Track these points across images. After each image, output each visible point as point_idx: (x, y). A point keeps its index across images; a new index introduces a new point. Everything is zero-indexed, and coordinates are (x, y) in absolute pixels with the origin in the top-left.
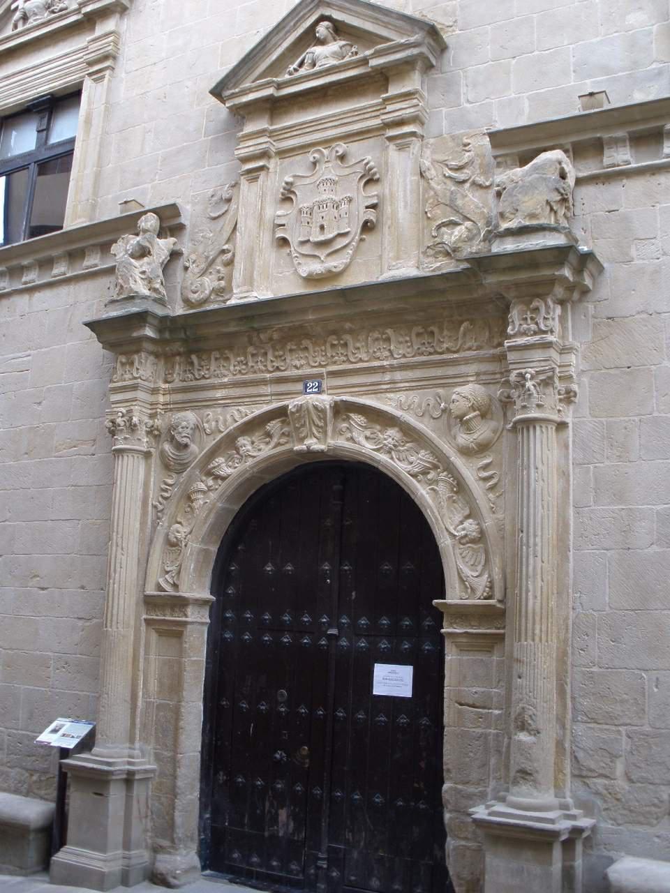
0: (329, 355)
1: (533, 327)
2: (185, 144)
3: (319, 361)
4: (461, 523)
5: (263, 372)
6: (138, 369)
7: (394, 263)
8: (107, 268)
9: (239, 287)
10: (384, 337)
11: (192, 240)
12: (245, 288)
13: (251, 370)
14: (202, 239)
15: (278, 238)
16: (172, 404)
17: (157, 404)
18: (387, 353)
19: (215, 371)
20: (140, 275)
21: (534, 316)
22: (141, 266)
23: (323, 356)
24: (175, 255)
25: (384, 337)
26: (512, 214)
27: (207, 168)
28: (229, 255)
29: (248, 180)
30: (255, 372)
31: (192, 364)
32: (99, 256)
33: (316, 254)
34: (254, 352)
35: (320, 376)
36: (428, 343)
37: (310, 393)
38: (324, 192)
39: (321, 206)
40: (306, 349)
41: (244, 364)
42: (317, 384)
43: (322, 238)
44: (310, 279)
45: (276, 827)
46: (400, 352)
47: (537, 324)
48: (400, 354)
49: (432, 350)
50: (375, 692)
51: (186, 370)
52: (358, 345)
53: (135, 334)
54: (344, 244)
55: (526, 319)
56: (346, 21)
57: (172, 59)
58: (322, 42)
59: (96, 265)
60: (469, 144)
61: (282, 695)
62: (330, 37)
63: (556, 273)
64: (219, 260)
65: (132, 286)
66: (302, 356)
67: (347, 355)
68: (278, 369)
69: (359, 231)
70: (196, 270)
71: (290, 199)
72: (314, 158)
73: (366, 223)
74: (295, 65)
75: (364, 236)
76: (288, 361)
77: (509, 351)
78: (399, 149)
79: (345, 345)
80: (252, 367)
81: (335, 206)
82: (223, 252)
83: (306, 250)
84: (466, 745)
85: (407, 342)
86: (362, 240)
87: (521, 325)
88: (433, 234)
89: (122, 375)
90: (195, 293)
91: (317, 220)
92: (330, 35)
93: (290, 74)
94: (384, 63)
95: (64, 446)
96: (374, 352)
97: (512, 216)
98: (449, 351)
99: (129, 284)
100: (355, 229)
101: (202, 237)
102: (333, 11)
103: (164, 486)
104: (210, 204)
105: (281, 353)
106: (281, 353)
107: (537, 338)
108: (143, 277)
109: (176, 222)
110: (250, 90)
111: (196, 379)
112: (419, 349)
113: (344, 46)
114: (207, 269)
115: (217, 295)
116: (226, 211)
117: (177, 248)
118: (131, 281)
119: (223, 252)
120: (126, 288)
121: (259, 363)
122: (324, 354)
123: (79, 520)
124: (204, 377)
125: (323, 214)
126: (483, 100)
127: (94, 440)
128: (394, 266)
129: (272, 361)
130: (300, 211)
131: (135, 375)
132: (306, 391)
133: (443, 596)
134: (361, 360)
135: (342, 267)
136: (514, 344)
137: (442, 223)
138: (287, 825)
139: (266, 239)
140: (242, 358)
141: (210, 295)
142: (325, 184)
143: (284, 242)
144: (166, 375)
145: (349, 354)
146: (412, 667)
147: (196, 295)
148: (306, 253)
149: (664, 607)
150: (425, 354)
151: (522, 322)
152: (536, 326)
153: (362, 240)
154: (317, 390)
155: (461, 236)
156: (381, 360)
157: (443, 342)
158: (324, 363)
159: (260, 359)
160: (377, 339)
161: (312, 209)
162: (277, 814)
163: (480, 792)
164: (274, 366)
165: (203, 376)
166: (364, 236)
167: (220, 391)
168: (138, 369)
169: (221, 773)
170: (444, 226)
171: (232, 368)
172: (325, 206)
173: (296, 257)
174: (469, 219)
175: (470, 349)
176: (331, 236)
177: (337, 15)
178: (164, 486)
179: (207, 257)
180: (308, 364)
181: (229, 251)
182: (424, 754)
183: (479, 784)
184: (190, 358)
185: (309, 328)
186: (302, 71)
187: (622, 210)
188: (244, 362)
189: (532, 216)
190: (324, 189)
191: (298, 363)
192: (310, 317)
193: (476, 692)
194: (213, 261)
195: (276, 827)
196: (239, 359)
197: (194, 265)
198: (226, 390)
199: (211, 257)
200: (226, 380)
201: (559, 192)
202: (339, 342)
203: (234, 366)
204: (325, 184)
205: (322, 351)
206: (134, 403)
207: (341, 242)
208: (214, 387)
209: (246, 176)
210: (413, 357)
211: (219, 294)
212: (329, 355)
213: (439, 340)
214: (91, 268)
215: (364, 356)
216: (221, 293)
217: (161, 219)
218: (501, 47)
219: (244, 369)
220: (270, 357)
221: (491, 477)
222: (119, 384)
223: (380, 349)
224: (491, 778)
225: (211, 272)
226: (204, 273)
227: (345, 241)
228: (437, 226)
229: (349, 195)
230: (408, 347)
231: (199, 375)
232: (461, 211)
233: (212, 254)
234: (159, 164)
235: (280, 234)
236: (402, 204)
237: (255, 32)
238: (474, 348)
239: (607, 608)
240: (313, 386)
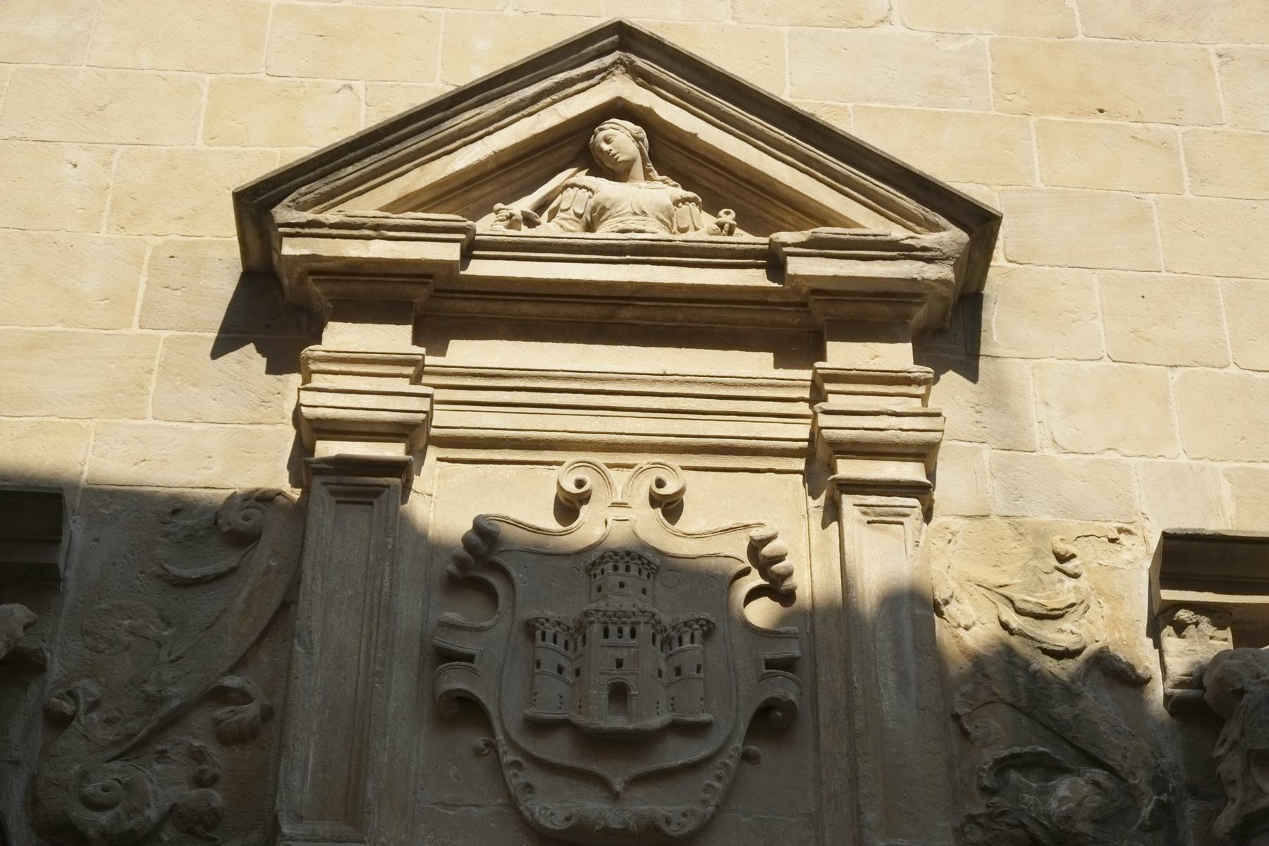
9: (299, 818)
11: (84, 633)
27: (150, 421)
28: (251, 711)
29: (333, 493)
33: (596, 768)
38: (618, 590)
43: (617, 722)
54: (696, 757)
58: (616, 172)
60: (1073, 556)
69: (743, 728)
70: (105, 735)
72: (580, 483)
73: (765, 711)
78: (869, 522)
81: (659, 638)
82: (220, 695)
83: (557, 749)
86: (748, 757)
88: (986, 782)
90: (101, 807)
94: (835, 278)
101: (132, 632)
104: (167, 535)
109: (476, 539)
114: (145, 742)
116: (232, 571)
125: (621, 654)
126: (1100, 453)
130: (530, 629)
137: (1013, 756)
141: (160, 825)
142: (622, 566)
147: (104, 818)
148: (558, 760)
155: (1080, 804)
172: (627, 630)
173: (517, 765)
179: (153, 701)
186: (547, 229)
194: (175, 719)
197: (94, 715)
199: (176, 703)
204: (622, 566)
207: (677, 752)
209: (333, 479)
218: (1134, 331)
227: (696, 750)
228: (997, 762)
229: (706, 615)
232: (1068, 735)
233: (177, 695)
235: (455, 680)
236: (892, 676)
237: (339, 84)
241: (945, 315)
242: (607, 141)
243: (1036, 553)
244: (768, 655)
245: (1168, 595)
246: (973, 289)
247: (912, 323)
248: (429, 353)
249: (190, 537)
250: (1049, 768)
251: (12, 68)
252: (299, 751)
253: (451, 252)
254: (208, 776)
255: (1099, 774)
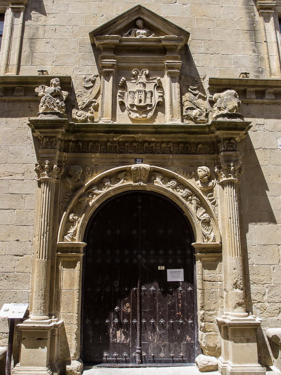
3: (140, 151)
4: (202, 215)
26: (224, 108)
37: (138, 163)
42: (141, 160)
45: (115, 339)
50: (168, 280)
55: (112, 149)
60: (197, 81)
61: (116, 283)
74: (127, 33)
84: (208, 296)
95: (4, 175)
102: (145, 17)
103: (66, 197)
123: (15, 209)
127: (23, 174)
132: (136, 162)
133: (195, 241)
138: (121, 337)
146: (167, 270)
149: (275, 244)
152: (233, 149)
154: (141, 162)
162: (116, 333)
163: (215, 313)
165: (85, 151)
169: (88, 319)
174: (199, 108)
177: (146, 18)
178: (66, 197)
182: (181, 301)
183: (214, 310)
184: (78, 144)
185: (136, 138)
187: (252, 113)
193: (211, 276)
195: (115, 339)
202: (167, 146)
221: (213, 199)
224: (219, 308)
237: (102, 15)
239: (257, 245)
240: (139, 161)
241: (182, 48)
242: (138, 23)
243: (193, 81)
244: (159, 95)
245: (151, 103)
246: (186, 43)
247: (178, 49)
248: (115, 55)
249: (87, 81)
250: (192, 109)
251: (59, 14)
252: (237, 281)
253: (117, 41)
254: (237, 148)
255: (199, 109)
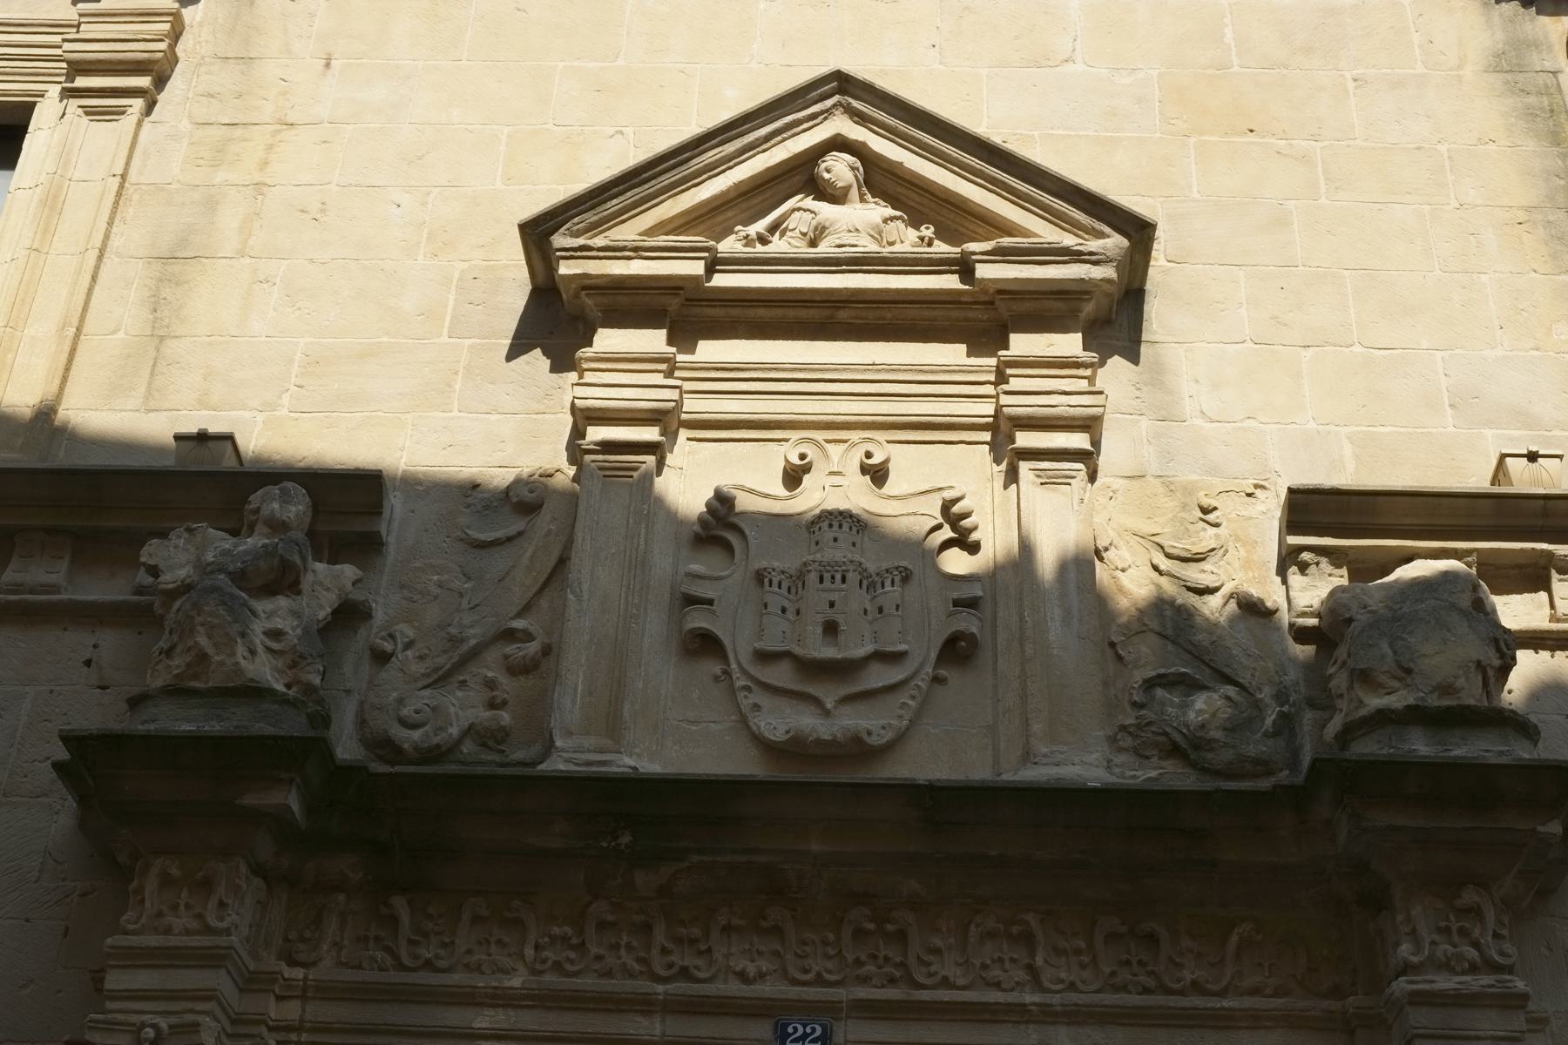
0: (850, 958)
1: (1472, 953)
2: (385, 339)
5: (632, 976)
6: (222, 904)
7: (1045, 750)
8: (93, 603)
10: (1015, 930)
11: (402, 587)
12: (589, 742)
13: (597, 966)
14: (438, 591)
15: (692, 631)
16: (308, 1031)
17: (258, 1023)
18: (1021, 975)
19: (469, 952)
20: (262, 637)
21: (1467, 925)
22: (270, 615)
23: (829, 957)
24: (349, 614)
25: (1015, 930)
26: (1395, 677)
28: (533, 647)
30: (609, 974)
31: (394, 920)
32: (64, 566)
34: (610, 918)
35: (830, 1010)
36: (1140, 962)
39: (827, 576)
40: (777, 931)
41: (573, 948)
43: (829, 653)
44: (794, 750)
46: (1063, 975)
47: (1476, 945)
48: (1062, 981)
49: (1151, 982)
51: (366, 939)
52: (937, 942)
53: (249, 800)
54: (893, 681)
56: (906, 165)
57: (350, 127)
58: (835, 196)
59: (53, 589)
60: (1215, 509)
62: (854, 192)
63: (1541, 829)
64: (493, 655)
65: (243, 662)
66: (762, 948)
67: (902, 965)
68: (685, 974)
69: (933, 655)
70: (417, 668)
71: (728, 548)
75: (942, 672)
76: (718, 956)
77: (1411, 1003)
78: (1042, 484)
79: (901, 937)
80: (599, 958)
81: (865, 583)
82: (509, 635)
83: (780, 675)
85: (1078, 952)
86: (937, 680)
87: (1433, 943)
89: (160, 914)
90: (414, 727)
91: (816, 599)
92: (855, 185)
93: (748, 241)
96: (984, 967)
97: (1396, 684)
98: (1197, 988)
99: (234, 654)
100: (923, 651)
101: (440, 585)
104: (468, 506)
105: (696, 932)
106: (696, 932)
107: (1486, 980)
108: (275, 646)
110: (637, 251)
111: (401, 967)
112: (1113, 974)
113: (892, 219)
115: (484, 745)
116: (520, 534)
117: (357, 596)
118: (241, 650)
119: (509, 635)
120: (221, 664)
121: (623, 952)
122: (832, 952)
124: (428, 965)
125: (835, 596)
128: (1045, 756)
129: (665, 951)
130: (760, 577)
131: (213, 922)
134: (946, 983)
135: (888, 736)
136: (1427, 987)
137: (1160, 676)
139: (654, 628)
140: (568, 929)
141: (460, 741)
142: (836, 524)
143: (705, 645)
144: (286, 940)
145: (912, 961)
147: (416, 735)
150: (1130, 987)
151: (1436, 937)
153: (937, 680)
156: (1004, 990)
157: (1180, 966)
158: (833, 978)
159: (625, 939)
160: (991, 935)
161: (801, 575)
164: (671, 966)
166: (942, 672)
167: (490, 1012)
168: (222, 904)
170: (1163, 686)
171: (529, 952)
172: (838, 577)
174: (1228, 680)
175: (1255, 991)
176: (860, 652)
179: (455, 641)
180: (784, 974)
181: (528, 636)
186: (778, 246)
188: (575, 941)
189: (1446, 689)
190: (833, 535)
191: (741, 964)
192: (815, 847)
194: (474, 654)
196: (556, 930)
197: (409, 653)
198: (511, 1012)
200: (516, 982)
201: (1498, 650)
203: (537, 947)
205: (825, 943)
206: (200, 1006)
207: (879, 676)
208: (469, 998)
210: (1098, 992)
211: (491, 743)
212: (850, 958)
213: (1171, 959)
214: (31, 592)
215: (951, 971)
216: (499, 743)
217: (316, 508)
219: (572, 962)
220: (660, 936)
222: (152, 940)
223: (1001, 960)
225: (463, 682)
226: (440, 679)
227: (894, 675)
228: (1145, 681)
229: (904, 563)
230: (1083, 966)
231: (416, 957)
232: (1206, 658)
233: (474, 635)
234: (295, 369)
235: (698, 620)
236: (1057, 612)
237: (612, 130)
238: (1268, 991)
